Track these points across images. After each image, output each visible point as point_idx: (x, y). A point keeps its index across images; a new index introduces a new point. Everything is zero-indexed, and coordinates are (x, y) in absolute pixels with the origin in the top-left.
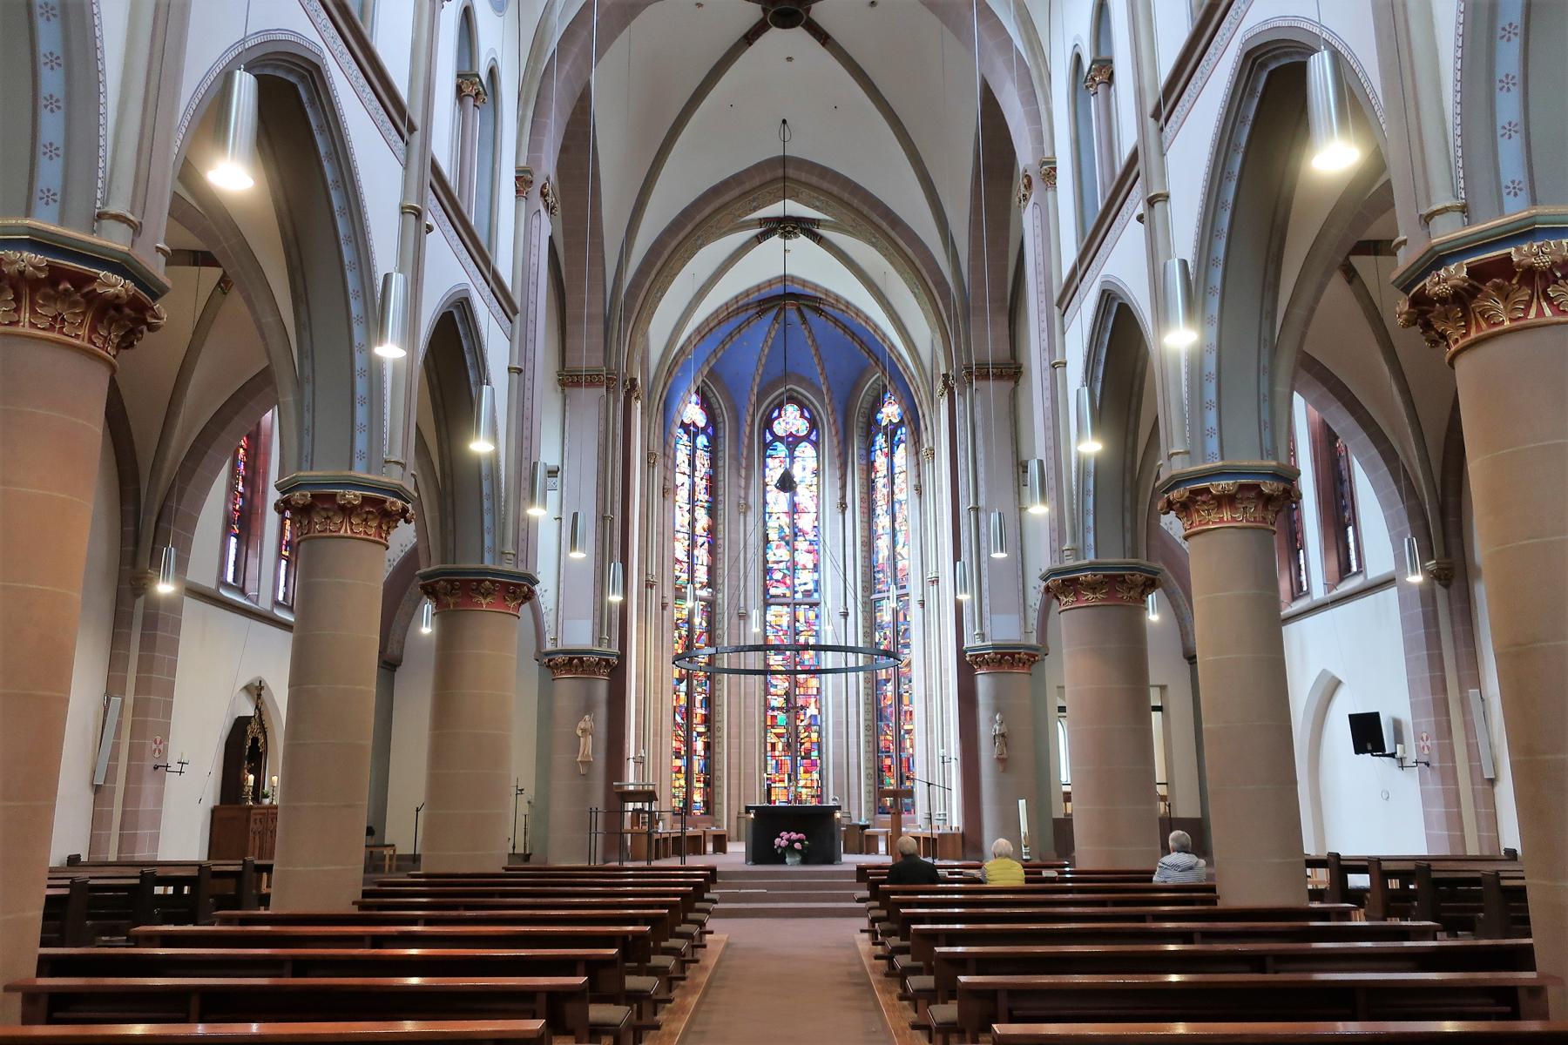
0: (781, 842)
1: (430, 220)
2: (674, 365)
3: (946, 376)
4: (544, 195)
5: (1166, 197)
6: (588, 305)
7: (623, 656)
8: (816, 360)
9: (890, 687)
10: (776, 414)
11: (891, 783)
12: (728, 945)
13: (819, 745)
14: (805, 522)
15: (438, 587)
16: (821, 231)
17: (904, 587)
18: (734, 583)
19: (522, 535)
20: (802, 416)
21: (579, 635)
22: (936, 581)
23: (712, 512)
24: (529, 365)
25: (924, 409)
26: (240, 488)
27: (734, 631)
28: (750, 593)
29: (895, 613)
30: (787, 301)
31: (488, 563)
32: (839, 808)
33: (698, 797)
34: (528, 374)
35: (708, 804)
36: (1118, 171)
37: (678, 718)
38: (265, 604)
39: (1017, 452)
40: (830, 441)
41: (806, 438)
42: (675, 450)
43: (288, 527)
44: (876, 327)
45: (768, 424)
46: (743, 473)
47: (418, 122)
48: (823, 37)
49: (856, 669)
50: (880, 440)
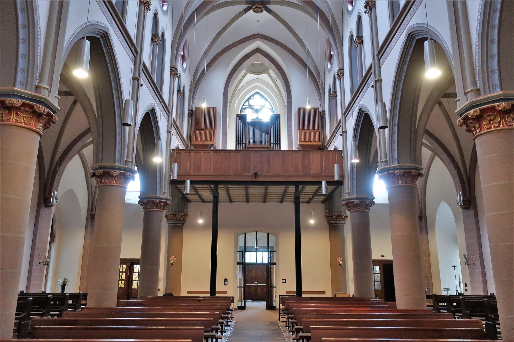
36: (364, 74)
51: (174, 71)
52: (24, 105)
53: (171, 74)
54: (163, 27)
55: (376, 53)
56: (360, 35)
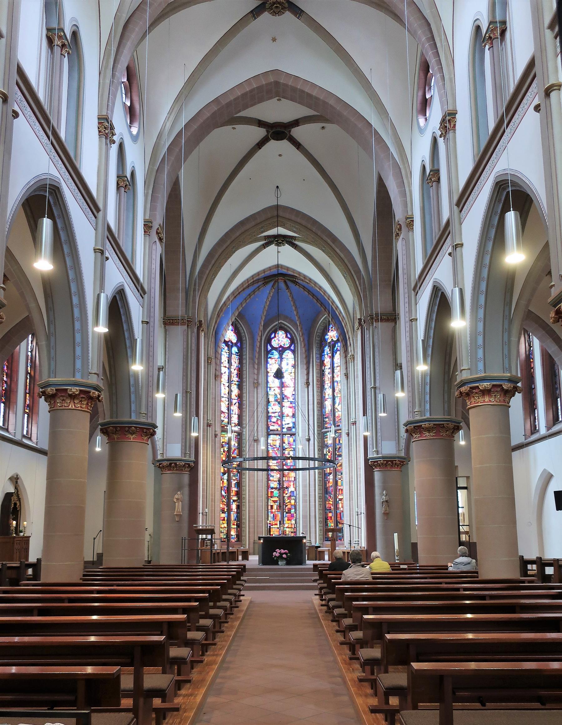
0: (276, 554)
1: (107, 255)
2: (220, 311)
3: (360, 320)
5: (462, 245)
7: (196, 462)
8: (294, 308)
9: (331, 477)
10: (273, 336)
11: (331, 525)
12: (251, 602)
13: (295, 506)
14: (288, 392)
15: (109, 430)
16: (296, 242)
17: (339, 426)
18: (251, 423)
19: (150, 404)
20: (287, 337)
21: (175, 451)
22: (355, 423)
23: (240, 387)
24: (152, 320)
25: (349, 335)
26: (5, 379)
29: (334, 439)
30: (278, 277)
31: (134, 418)
32: (305, 537)
33: (233, 533)
34: (152, 324)
35: (239, 536)
36: (442, 229)
37: (223, 493)
38: (18, 437)
39: (395, 359)
41: (289, 348)
42: (221, 355)
43: (28, 397)
44: (325, 292)
45: (269, 341)
47: (101, 205)
48: (297, 145)
49: (314, 468)
50: (327, 349)
51: (106, 128)
53: (145, 232)
54: (121, 134)
55: (455, 198)
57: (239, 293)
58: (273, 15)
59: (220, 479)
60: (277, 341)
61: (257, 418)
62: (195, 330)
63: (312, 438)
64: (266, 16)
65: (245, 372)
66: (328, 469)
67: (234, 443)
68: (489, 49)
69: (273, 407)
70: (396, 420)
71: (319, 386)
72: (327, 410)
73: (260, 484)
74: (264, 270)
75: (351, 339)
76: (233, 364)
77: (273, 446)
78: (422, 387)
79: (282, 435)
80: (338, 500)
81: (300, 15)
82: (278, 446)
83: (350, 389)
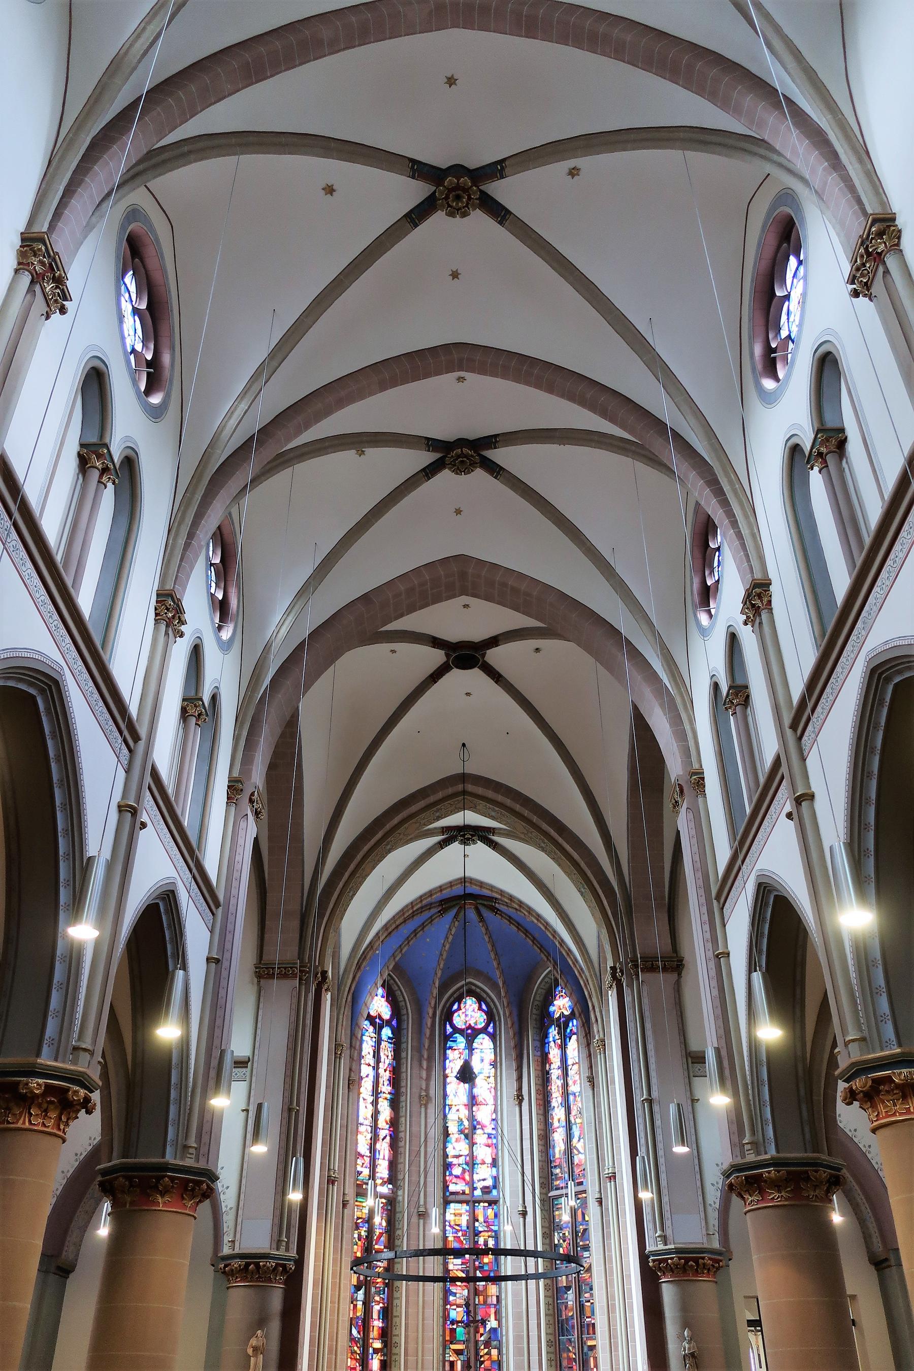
1: (145, 818)
2: (362, 959)
4: (251, 801)
6: (284, 900)
7: (300, 1262)
8: (493, 956)
9: (571, 1295)
10: (455, 1007)
14: (484, 1114)
16: (496, 838)
17: (581, 1183)
19: (206, 1128)
20: (480, 1008)
21: (254, 1236)
22: (613, 1177)
23: (395, 1104)
24: (227, 955)
27: (413, 1232)
28: (430, 1189)
29: (574, 1212)
30: (466, 901)
31: (169, 1158)
34: (225, 964)
36: (762, 780)
37: (354, 1332)
40: (507, 1033)
41: (484, 1030)
44: (547, 925)
45: (448, 1016)
46: (425, 1064)
47: (143, 732)
49: (537, 1276)
50: (553, 1032)
51: (169, 611)
52: (49, 1089)
53: (228, 798)
55: (787, 720)
56: (739, 682)
57: (397, 927)
58: (457, 474)
59: (348, 1300)
60: (463, 1017)
61: (426, 1162)
62: (313, 988)
63: (530, 1210)
64: (439, 218)
65: (404, 1075)
66: (564, 1277)
67: (379, 1221)
68: (820, 472)
69: (455, 1145)
70: (697, 1168)
71: (541, 1102)
72: (557, 1150)
73: (428, 1312)
74: (440, 887)
75: (597, 1010)
76: (382, 1060)
77: (456, 1227)
78: (753, 1088)
79: (473, 1203)
80: (586, 1349)
81: (498, 473)
82: (464, 1228)
83: (599, 1107)
